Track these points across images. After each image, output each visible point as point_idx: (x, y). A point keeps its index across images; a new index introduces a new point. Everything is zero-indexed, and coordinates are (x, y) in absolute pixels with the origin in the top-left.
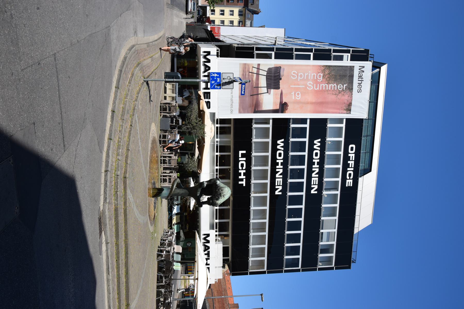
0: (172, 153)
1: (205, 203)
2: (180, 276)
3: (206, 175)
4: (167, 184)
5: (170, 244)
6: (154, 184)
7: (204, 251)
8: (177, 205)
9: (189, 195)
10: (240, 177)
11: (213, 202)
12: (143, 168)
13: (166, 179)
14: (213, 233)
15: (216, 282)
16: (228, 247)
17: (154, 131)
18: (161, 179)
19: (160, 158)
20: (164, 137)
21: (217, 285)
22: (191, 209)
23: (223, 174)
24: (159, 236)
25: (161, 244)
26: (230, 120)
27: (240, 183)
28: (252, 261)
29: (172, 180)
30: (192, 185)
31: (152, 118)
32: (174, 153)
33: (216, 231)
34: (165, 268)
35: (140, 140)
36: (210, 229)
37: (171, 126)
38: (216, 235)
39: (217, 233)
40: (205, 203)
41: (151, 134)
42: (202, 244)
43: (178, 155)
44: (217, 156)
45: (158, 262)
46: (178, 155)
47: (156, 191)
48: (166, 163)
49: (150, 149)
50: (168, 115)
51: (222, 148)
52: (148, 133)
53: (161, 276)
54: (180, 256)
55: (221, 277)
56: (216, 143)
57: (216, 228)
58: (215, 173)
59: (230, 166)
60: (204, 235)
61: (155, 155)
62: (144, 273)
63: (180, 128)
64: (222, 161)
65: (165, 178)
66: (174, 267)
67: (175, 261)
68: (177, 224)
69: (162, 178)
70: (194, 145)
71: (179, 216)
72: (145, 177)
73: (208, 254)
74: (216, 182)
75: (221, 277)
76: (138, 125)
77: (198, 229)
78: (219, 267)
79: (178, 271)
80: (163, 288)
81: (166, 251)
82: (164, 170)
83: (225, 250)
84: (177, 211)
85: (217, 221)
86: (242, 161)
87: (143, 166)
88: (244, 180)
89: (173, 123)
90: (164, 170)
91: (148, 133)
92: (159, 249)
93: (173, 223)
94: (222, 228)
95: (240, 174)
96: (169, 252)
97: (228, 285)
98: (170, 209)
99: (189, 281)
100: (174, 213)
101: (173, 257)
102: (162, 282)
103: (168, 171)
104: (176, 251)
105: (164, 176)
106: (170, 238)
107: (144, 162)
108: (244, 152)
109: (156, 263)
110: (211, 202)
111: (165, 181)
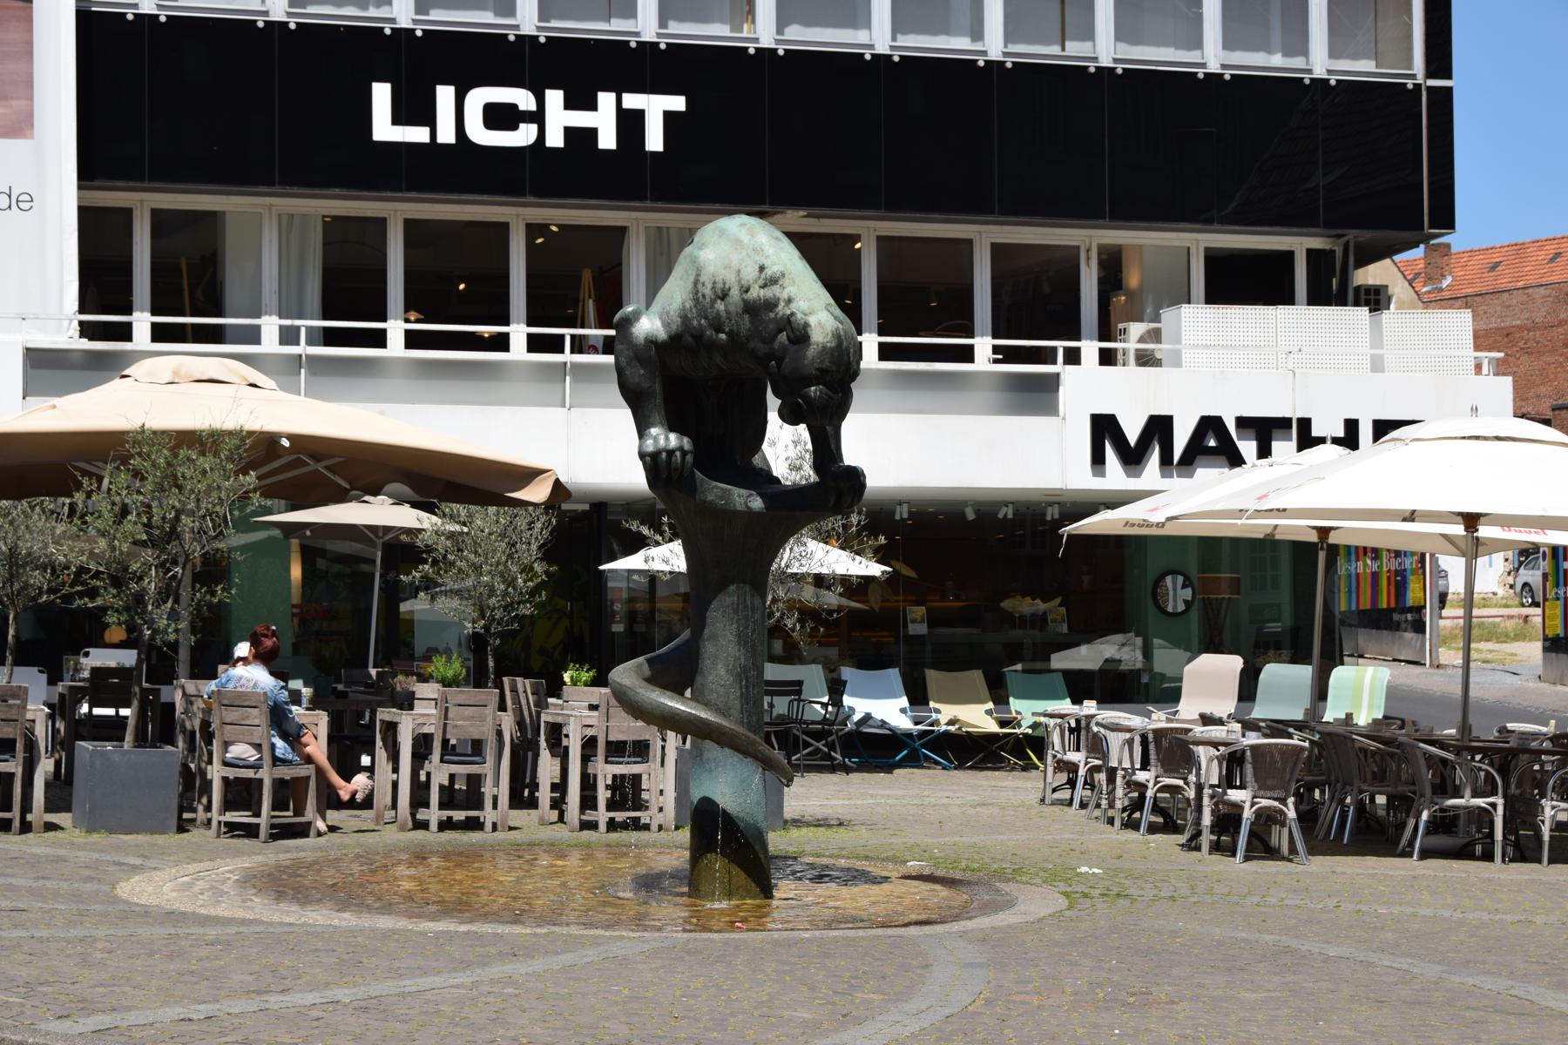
0: (391, 728)
1: (826, 449)
2: (1436, 675)
3: (592, 443)
4: (660, 782)
5: (1172, 750)
6: (650, 883)
7: (1236, 460)
8: (836, 689)
9: (760, 587)
10: (608, 140)
11: (821, 376)
12: (521, 969)
13: (618, 783)
14: (1089, 385)
15: (1500, 369)
16: (1214, 260)
17: (192, 880)
18: (612, 825)
19: (432, 837)
20: (241, 793)
21: (1525, 364)
22: (876, 569)
23: (578, 289)
24: (1098, 843)
25: (1170, 826)
26: (88, 218)
27: (655, 140)
28: (1334, 53)
29: (627, 728)
30: (668, 557)
31: (76, 896)
32: (384, 714)
33: (1073, 357)
34: (1365, 797)
35: (275, 1001)
36: (1050, 409)
37: (141, 740)
38: (1107, 358)
39: (1090, 349)
40: (826, 449)
41: (221, 911)
42: (1176, 483)
43: (401, 682)
44: (413, 340)
45: (1313, 851)
46: (401, 682)
47: (717, 863)
48: (475, 781)
49: (347, 919)
50: (45, 767)
51: (349, 295)
52: (212, 932)
53: (1435, 826)
54: (1275, 673)
55: (1460, 323)
56: (303, 349)
57: (1047, 356)
58: (567, 357)
59: (503, 229)
60: (1098, 459)
61: (406, 878)
62: (1403, 963)
63: (160, 664)
64: (457, 298)
65: (603, 795)
66: (1362, 719)
67: (1315, 712)
68: (998, 693)
69: (602, 815)
70: (315, 542)
71: (932, 675)
72: (591, 954)
73: (1265, 430)
74: (651, 342)
75: (1460, 323)
76: (132, 1018)
77: (1052, 513)
78: (1377, 338)
79: (1393, 694)
80: (1536, 809)
81: (1228, 782)
82: (533, 803)
83: (1242, 282)
84: (1063, 698)
85: (983, 345)
86: (462, 115)
87: (497, 970)
88: (632, 101)
89: (121, 722)
90: (533, 803)
91: (212, 932)
92: (1206, 839)
93: (992, 727)
94: (1042, 311)
95: (581, 138)
96: (1234, 761)
97: (1533, 271)
98: (877, 751)
99: (1486, 603)
100: (904, 723)
101: (1278, 728)
102: (1484, 816)
103: (547, 769)
104: (1225, 706)
105: (588, 802)
106: (1118, 752)
107: (466, 965)
108: (382, 93)
109: (1321, 864)
110: (823, 397)
111: (627, 794)
